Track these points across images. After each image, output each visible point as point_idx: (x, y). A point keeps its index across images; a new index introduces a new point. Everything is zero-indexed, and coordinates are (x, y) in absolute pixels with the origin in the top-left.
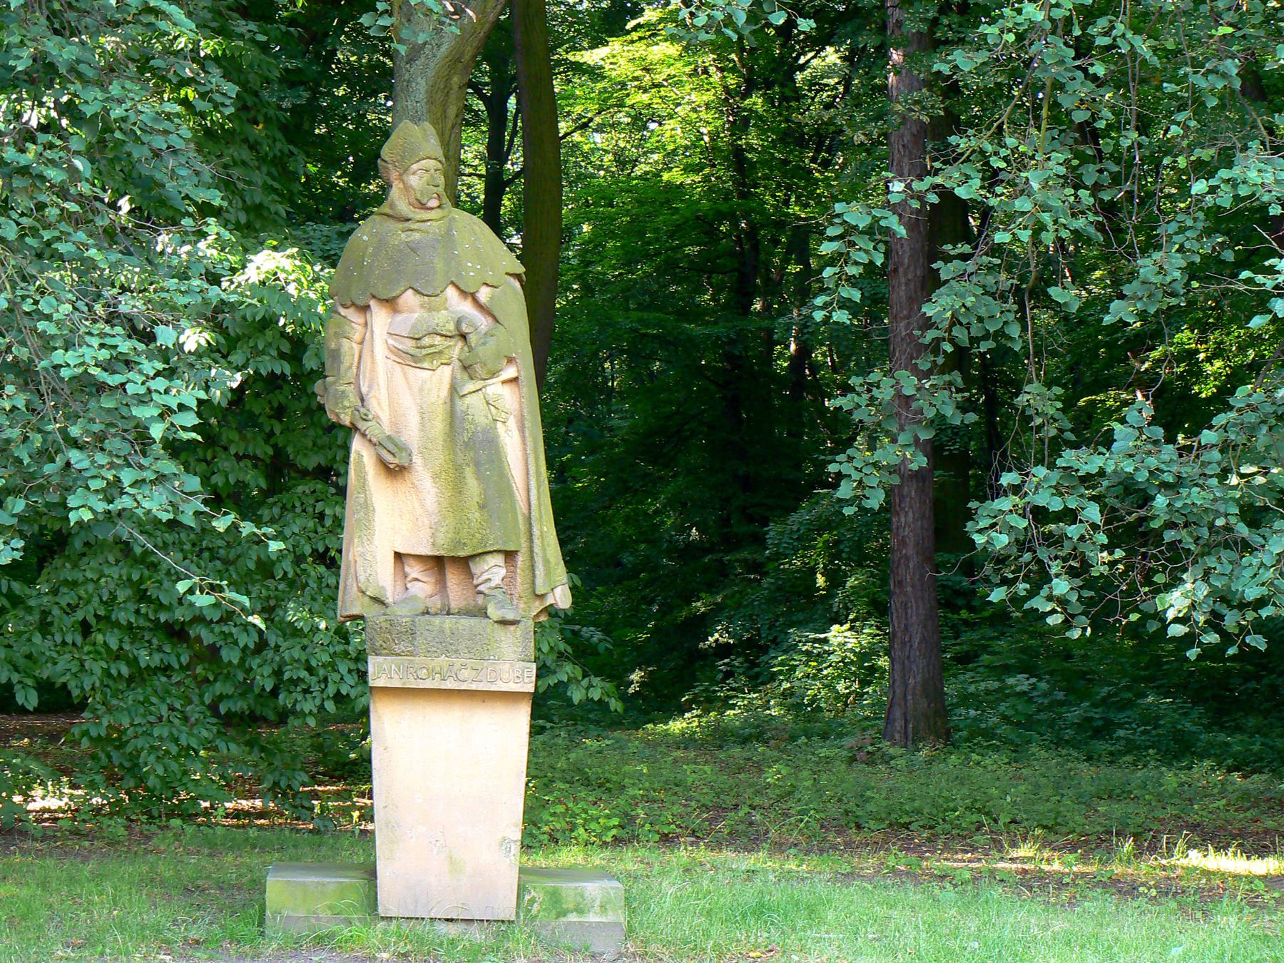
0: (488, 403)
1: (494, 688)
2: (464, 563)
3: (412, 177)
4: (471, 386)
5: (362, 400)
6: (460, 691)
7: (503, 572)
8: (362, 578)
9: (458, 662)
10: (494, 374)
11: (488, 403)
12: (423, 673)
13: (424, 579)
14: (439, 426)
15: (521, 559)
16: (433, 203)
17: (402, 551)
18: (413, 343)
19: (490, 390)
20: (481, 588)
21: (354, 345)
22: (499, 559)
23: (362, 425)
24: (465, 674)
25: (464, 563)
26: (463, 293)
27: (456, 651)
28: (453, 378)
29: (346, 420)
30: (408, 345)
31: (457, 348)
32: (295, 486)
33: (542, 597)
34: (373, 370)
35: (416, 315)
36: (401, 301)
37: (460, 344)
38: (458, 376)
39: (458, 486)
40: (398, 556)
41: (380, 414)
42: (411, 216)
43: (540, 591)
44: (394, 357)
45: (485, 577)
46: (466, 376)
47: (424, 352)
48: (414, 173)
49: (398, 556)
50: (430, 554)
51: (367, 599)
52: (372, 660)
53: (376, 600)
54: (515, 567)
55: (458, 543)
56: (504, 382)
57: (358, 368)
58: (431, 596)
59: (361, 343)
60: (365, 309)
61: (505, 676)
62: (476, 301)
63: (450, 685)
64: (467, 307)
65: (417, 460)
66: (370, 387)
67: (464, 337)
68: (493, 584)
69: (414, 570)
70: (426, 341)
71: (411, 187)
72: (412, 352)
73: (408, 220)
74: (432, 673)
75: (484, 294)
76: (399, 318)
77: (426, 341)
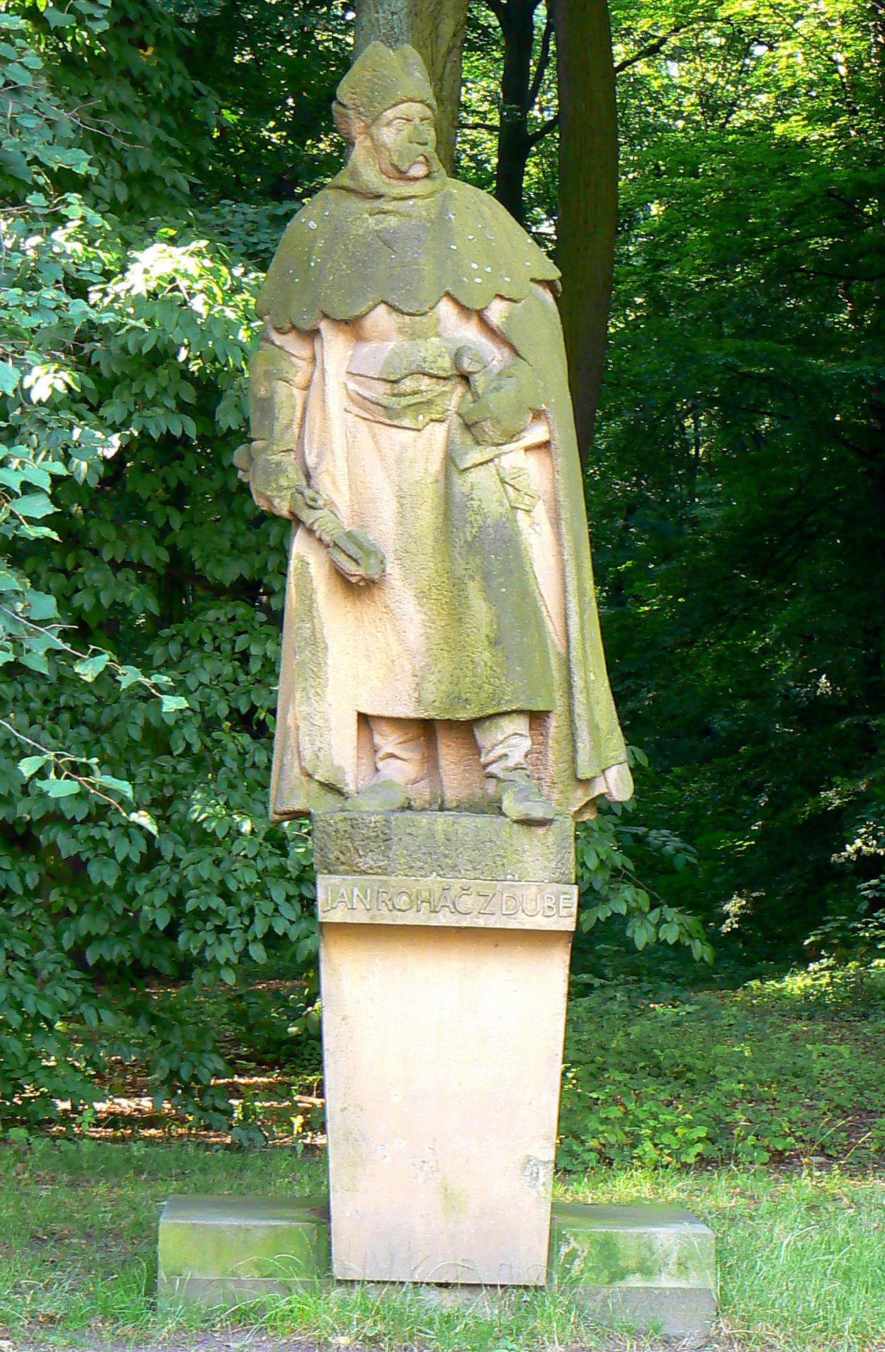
0: (503, 482)
2: (466, 730)
3: (385, 130)
4: (476, 455)
5: (308, 476)
7: (526, 744)
8: (307, 754)
9: (456, 884)
10: (512, 436)
11: (503, 482)
14: (426, 516)
17: (370, 712)
19: (506, 461)
20: (493, 769)
21: (295, 391)
22: (521, 724)
23: (307, 516)
24: (467, 902)
25: (466, 730)
26: (465, 310)
28: (449, 443)
29: (283, 508)
30: (379, 391)
33: (587, 783)
34: (325, 430)
35: (391, 345)
36: (368, 323)
37: (460, 390)
38: (457, 440)
39: (456, 612)
41: (335, 497)
42: (383, 190)
44: (357, 410)
45: (499, 751)
47: (404, 401)
50: (414, 715)
51: (315, 786)
54: (546, 736)
55: (458, 700)
57: (302, 426)
58: (415, 782)
60: (312, 335)
61: (530, 906)
63: (444, 919)
64: (470, 333)
65: (393, 569)
66: (320, 456)
67: (465, 378)
68: (511, 763)
69: (388, 741)
70: (408, 385)
72: (384, 402)
73: (379, 197)
74: (416, 900)
75: (497, 313)
76: (365, 349)
77: (408, 385)
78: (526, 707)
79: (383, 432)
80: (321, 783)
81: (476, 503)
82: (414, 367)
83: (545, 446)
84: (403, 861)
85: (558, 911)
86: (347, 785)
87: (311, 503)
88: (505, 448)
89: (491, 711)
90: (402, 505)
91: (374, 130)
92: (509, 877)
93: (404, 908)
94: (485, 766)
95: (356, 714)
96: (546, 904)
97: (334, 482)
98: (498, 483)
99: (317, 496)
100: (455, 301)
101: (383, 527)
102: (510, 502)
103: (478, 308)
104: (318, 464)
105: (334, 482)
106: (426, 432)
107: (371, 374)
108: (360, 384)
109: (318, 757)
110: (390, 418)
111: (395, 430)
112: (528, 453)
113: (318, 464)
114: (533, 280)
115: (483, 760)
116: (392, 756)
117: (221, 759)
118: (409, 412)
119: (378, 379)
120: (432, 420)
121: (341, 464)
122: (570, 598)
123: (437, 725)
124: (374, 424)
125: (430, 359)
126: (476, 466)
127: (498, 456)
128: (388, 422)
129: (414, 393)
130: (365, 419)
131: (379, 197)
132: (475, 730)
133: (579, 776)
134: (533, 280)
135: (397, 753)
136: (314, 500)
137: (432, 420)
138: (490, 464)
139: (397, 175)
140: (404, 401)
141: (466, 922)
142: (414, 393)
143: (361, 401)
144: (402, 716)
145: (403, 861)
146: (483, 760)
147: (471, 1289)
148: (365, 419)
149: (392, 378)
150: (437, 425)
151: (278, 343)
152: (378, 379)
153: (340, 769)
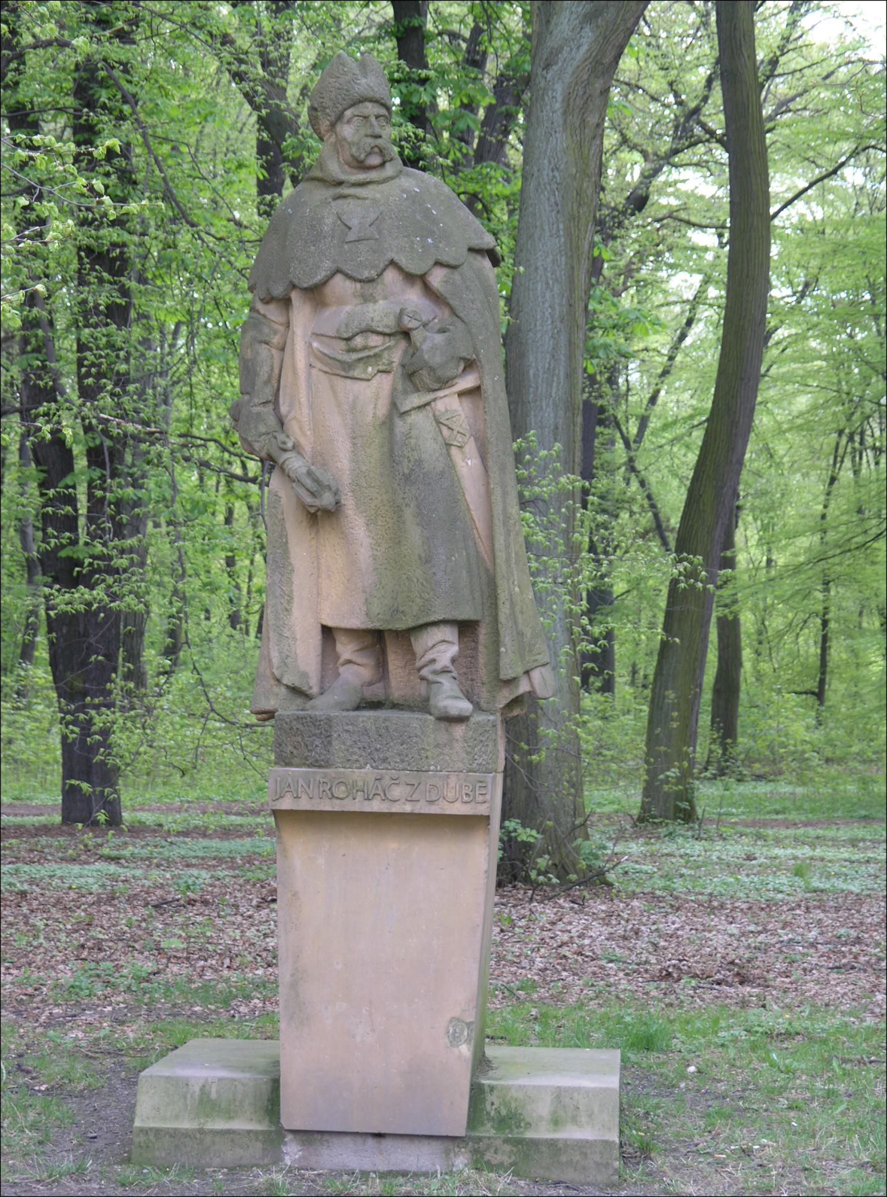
0: (438, 422)
1: (434, 810)
2: (405, 636)
4: (416, 400)
5: (281, 423)
6: (392, 814)
7: (454, 650)
9: (387, 775)
10: (445, 383)
11: (438, 422)
12: (340, 791)
13: (359, 660)
14: (374, 453)
15: (483, 633)
16: (375, 160)
17: (330, 623)
18: (343, 345)
19: (440, 406)
20: (425, 672)
21: (274, 351)
22: (449, 633)
24: (397, 792)
25: (405, 636)
26: (410, 277)
27: (385, 760)
28: (394, 390)
30: (338, 350)
31: (397, 354)
32: (815, 408)
33: (510, 682)
35: (348, 308)
36: (328, 290)
37: (403, 344)
39: (397, 538)
40: (327, 632)
41: (303, 441)
42: (343, 177)
43: (507, 673)
44: (319, 365)
45: (429, 656)
46: (410, 387)
47: (355, 356)
48: (349, 122)
49: (327, 632)
50: (363, 626)
52: (635, 812)
53: (295, 691)
54: (476, 642)
55: (395, 612)
56: (461, 394)
57: (279, 381)
58: (370, 684)
59: (283, 349)
60: (286, 302)
61: (451, 795)
62: (427, 289)
63: (376, 806)
64: (413, 297)
65: (349, 502)
66: (291, 405)
67: (406, 334)
68: (438, 666)
69: (346, 649)
70: (359, 341)
71: (345, 139)
72: (339, 357)
74: (352, 790)
75: (437, 278)
76: (328, 313)
77: (359, 341)
78: (449, 616)
79: (341, 383)
80: (288, 687)
81: (413, 441)
82: (363, 325)
83: (475, 392)
84: (341, 754)
85: (475, 797)
86: (311, 688)
87: (282, 446)
88: (441, 394)
89: (421, 622)
90: (354, 444)
91: (338, 128)
92: (432, 768)
93: (341, 796)
94: (420, 669)
95: (319, 628)
96: (464, 792)
97: (301, 428)
98: (434, 424)
99: (287, 440)
100: (400, 269)
101: (339, 465)
102: (444, 439)
103: (419, 272)
104: (289, 412)
105: (301, 428)
106: (374, 382)
107: (330, 334)
108: (322, 343)
109: (285, 664)
110: (344, 370)
111: (349, 381)
112: (464, 399)
113: (289, 412)
114: (471, 250)
115: (419, 664)
116: (349, 662)
117: (382, 665)
118: (361, 365)
119: (335, 338)
120: (379, 371)
121: (305, 411)
122: (496, 521)
123: (386, 635)
124: (334, 378)
125: (377, 319)
126: (414, 409)
127: (435, 400)
128: (343, 373)
129: (365, 348)
130: (326, 372)
131: (340, 183)
132: (412, 639)
133: (502, 677)
134: (471, 250)
135: (354, 659)
136: (284, 443)
137: (379, 371)
138: (428, 408)
139: (355, 164)
140: (355, 356)
141: (396, 808)
142: (365, 348)
143: (324, 358)
144: (354, 627)
145: (341, 754)
146: (419, 664)
147: (359, 1140)
148: (326, 372)
149: (345, 336)
150: (384, 375)
151: (262, 312)
152: (335, 338)
153: (304, 675)
